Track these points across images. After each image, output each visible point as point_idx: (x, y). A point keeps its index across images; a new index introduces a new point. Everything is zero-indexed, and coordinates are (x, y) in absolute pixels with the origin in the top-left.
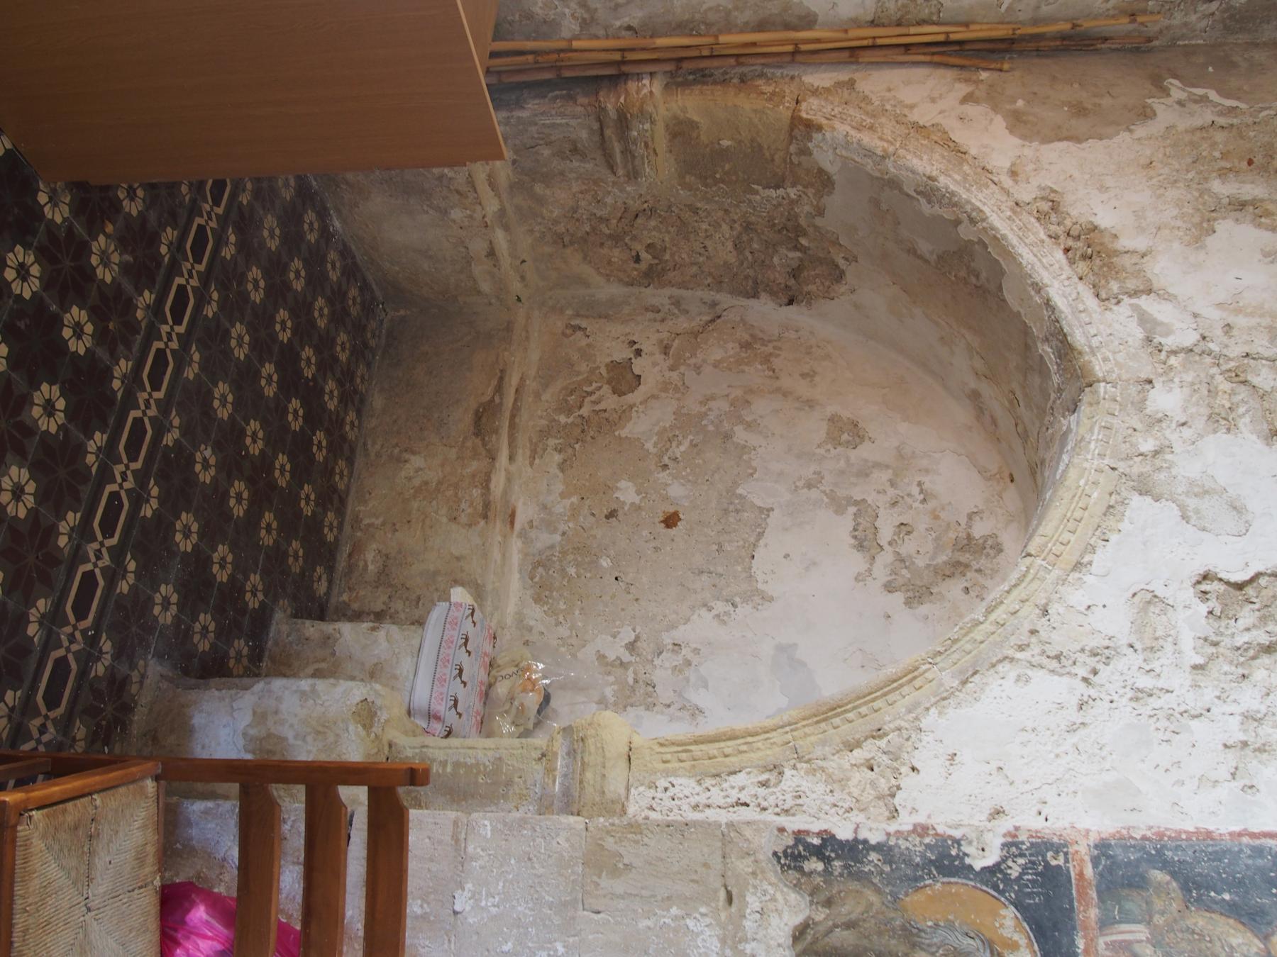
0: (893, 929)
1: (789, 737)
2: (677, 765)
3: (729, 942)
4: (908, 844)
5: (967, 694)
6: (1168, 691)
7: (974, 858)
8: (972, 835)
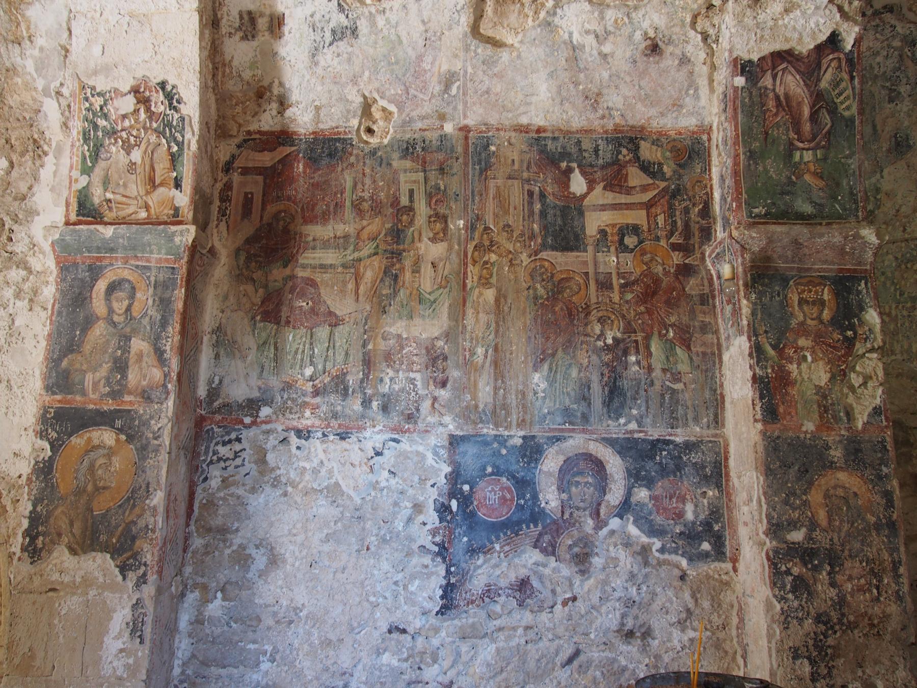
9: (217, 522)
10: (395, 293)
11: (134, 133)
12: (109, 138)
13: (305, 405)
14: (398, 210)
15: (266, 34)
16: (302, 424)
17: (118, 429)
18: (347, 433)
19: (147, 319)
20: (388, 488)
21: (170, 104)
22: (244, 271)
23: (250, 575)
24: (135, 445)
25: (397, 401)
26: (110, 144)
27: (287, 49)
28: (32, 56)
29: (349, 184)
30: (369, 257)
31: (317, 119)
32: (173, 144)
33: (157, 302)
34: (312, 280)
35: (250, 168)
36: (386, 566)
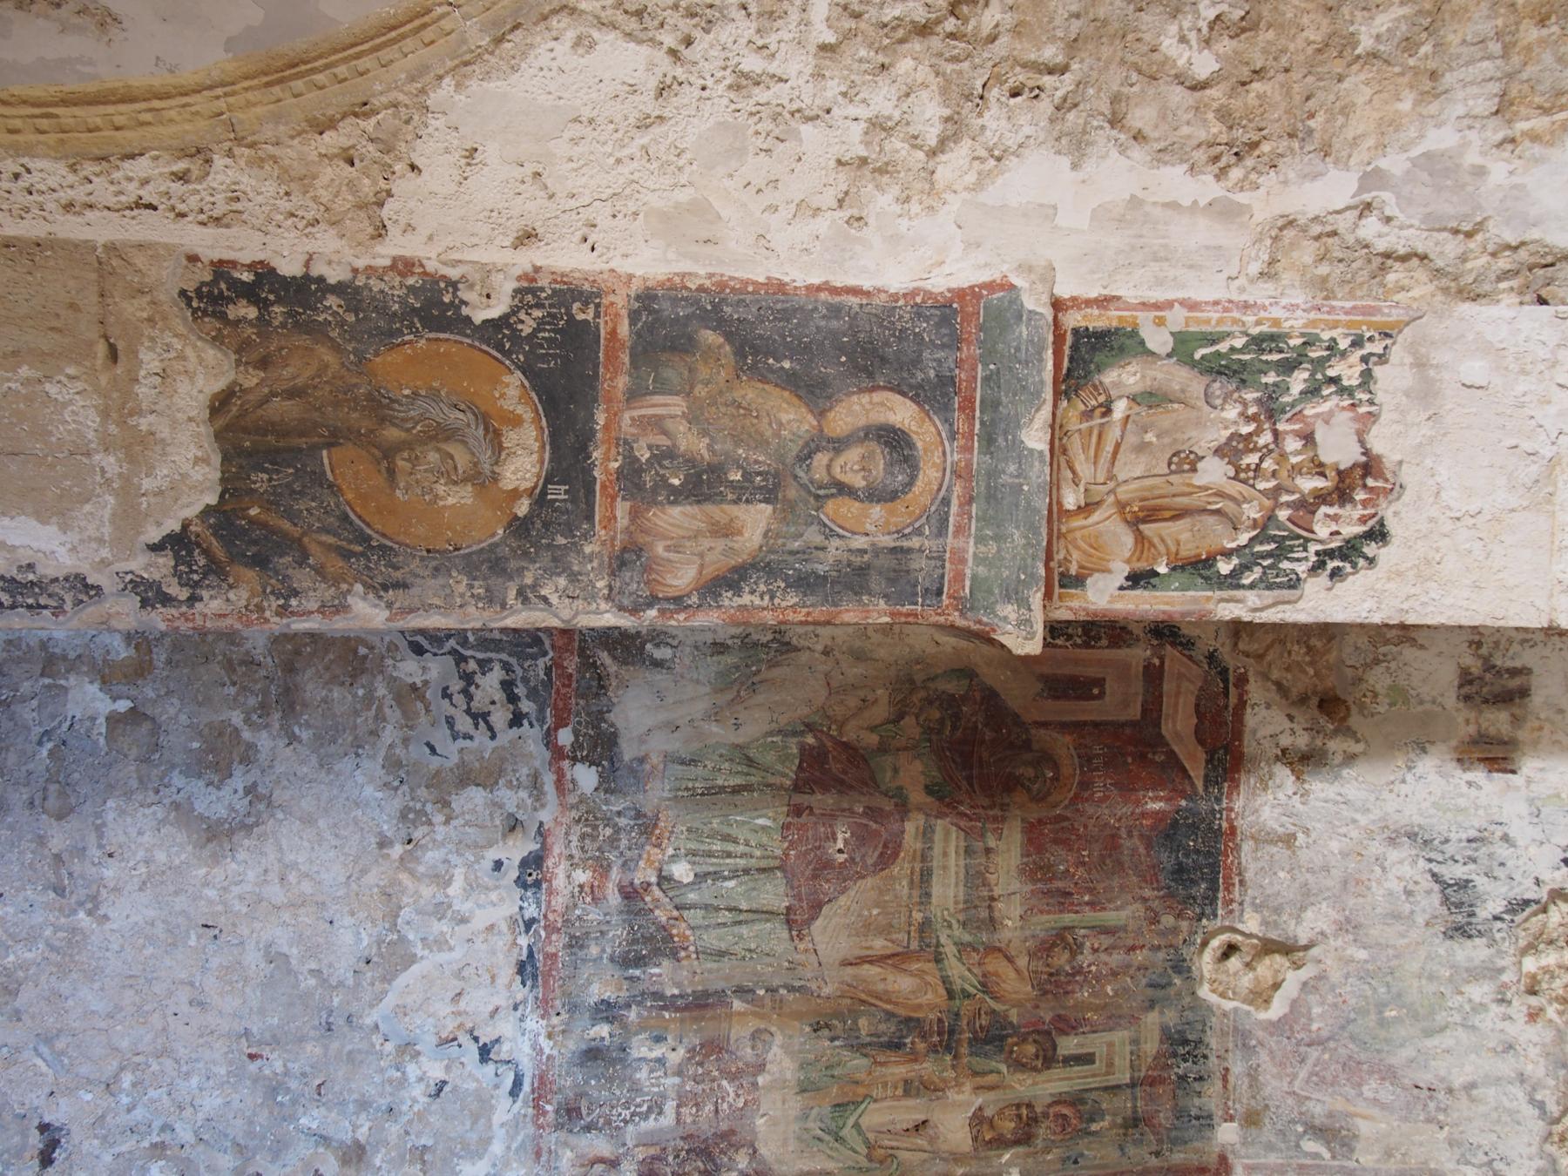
0: (355, 399)
1: (221, 104)
2: (33, 137)
3: (114, 415)
4: (383, 286)
5: (502, 59)
6: (781, 80)
7: (475, 307)
8: (475, 277)
9: (310, 687)
10: (859, 1048)
11: (1268, 464)
12: (1259, 401)
13: (603, 869)
14: (1048, 1033)
15: (1472, 729)
16: (556, 865)
17: (544, 493)
18: (535, 977)
19: (818, 540)
20: (403, 1082)
21: (1331, 554)
22: (922, 694)
23: (177, 780)
24: (504, 539)
25: (611, 1080)
26: (1245, 404)
27: (1433, 777)
28: (1465, 145)
29: (1111, 917)
30: (945, 980)
31: (1265, 838)
32: (1235, 561)
33: (857, 560)
34: (896, 855)
35: (1161, 685)
36: (211, 1103)
